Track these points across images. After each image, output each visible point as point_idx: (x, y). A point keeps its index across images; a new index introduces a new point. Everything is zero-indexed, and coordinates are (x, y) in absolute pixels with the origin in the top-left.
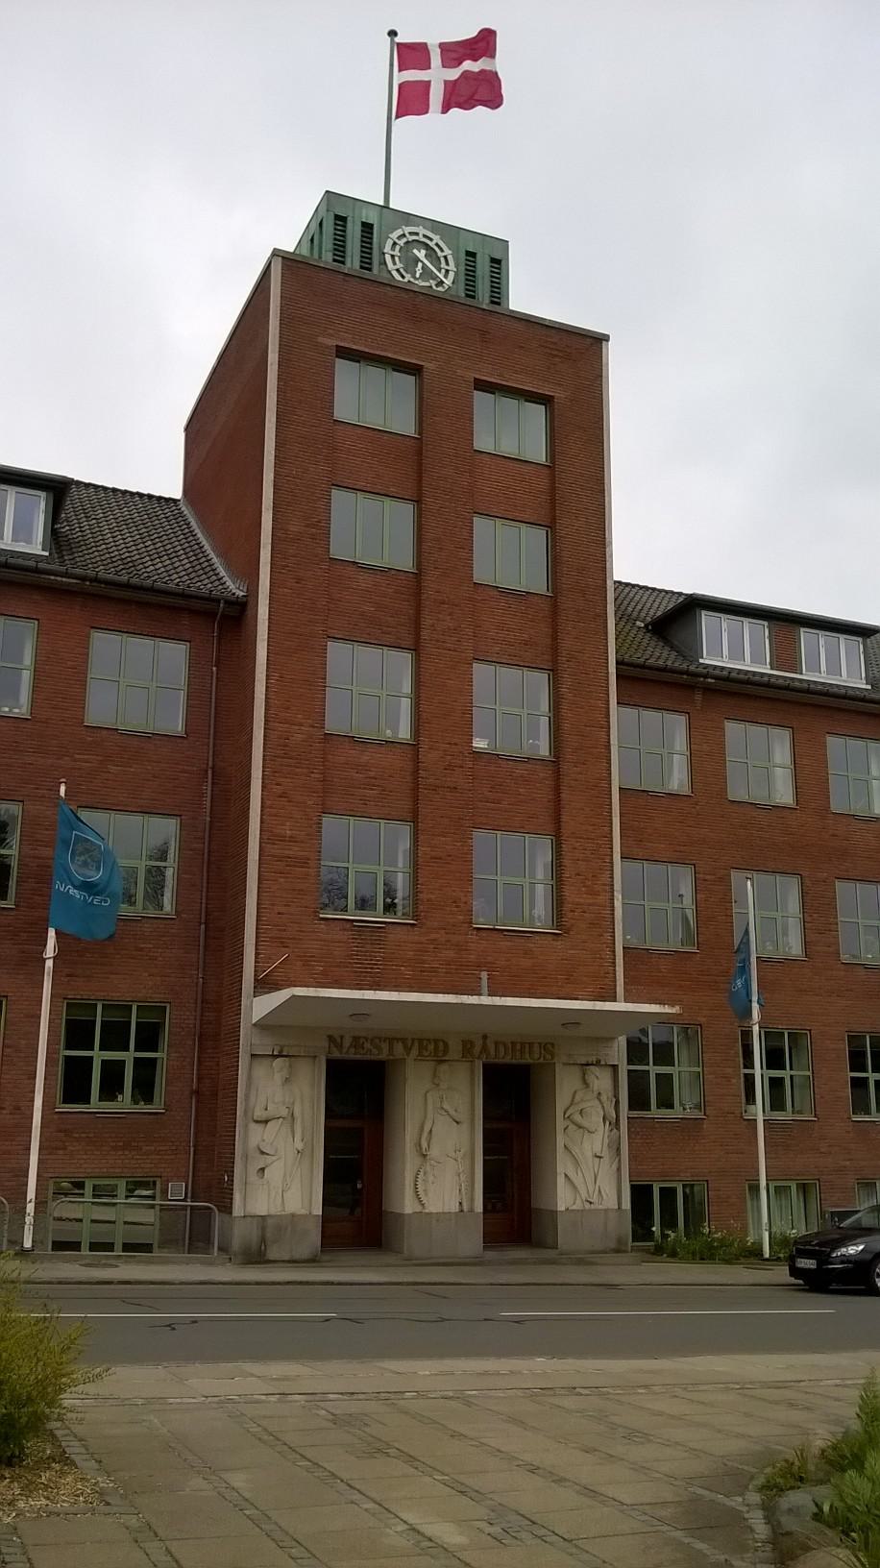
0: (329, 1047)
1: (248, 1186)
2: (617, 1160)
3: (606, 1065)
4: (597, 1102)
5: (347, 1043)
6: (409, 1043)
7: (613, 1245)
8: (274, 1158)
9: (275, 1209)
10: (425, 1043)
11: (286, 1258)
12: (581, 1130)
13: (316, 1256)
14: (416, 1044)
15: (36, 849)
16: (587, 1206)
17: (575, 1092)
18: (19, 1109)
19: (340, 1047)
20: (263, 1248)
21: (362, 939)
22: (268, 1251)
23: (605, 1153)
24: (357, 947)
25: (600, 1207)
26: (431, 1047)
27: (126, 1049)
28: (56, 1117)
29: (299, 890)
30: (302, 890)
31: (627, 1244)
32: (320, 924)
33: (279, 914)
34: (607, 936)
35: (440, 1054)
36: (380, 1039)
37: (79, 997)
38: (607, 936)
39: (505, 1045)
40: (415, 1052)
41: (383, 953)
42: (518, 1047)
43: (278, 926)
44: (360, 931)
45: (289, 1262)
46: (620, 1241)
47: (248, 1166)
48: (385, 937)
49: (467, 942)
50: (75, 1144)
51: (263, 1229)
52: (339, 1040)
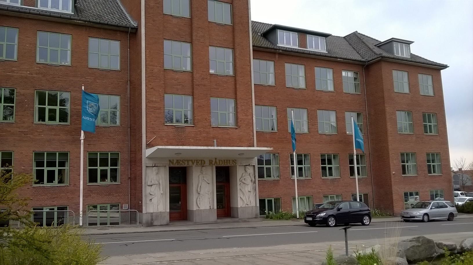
0: (170, 163)
4: (249, 176)
5: (175, 162)
6: (193, 161)
7: (254, 216)
8: (155, 196)
10: (198, 161)
12: (245, 184)
13: (168, 223)
14: (196, 161)
15: (75, 106)
16: (247, 206)
20: (152, 222)
22: (154, 223)
23: (252, 191)
26: (200, 162)
33: (153, 124)
35: (203, 164)
36: (185, 160)
40: (195, 164)
42: (226, 161)
44: (177, 129)
45: (160, 225)
46: (256, 215)
51: (152, 216)
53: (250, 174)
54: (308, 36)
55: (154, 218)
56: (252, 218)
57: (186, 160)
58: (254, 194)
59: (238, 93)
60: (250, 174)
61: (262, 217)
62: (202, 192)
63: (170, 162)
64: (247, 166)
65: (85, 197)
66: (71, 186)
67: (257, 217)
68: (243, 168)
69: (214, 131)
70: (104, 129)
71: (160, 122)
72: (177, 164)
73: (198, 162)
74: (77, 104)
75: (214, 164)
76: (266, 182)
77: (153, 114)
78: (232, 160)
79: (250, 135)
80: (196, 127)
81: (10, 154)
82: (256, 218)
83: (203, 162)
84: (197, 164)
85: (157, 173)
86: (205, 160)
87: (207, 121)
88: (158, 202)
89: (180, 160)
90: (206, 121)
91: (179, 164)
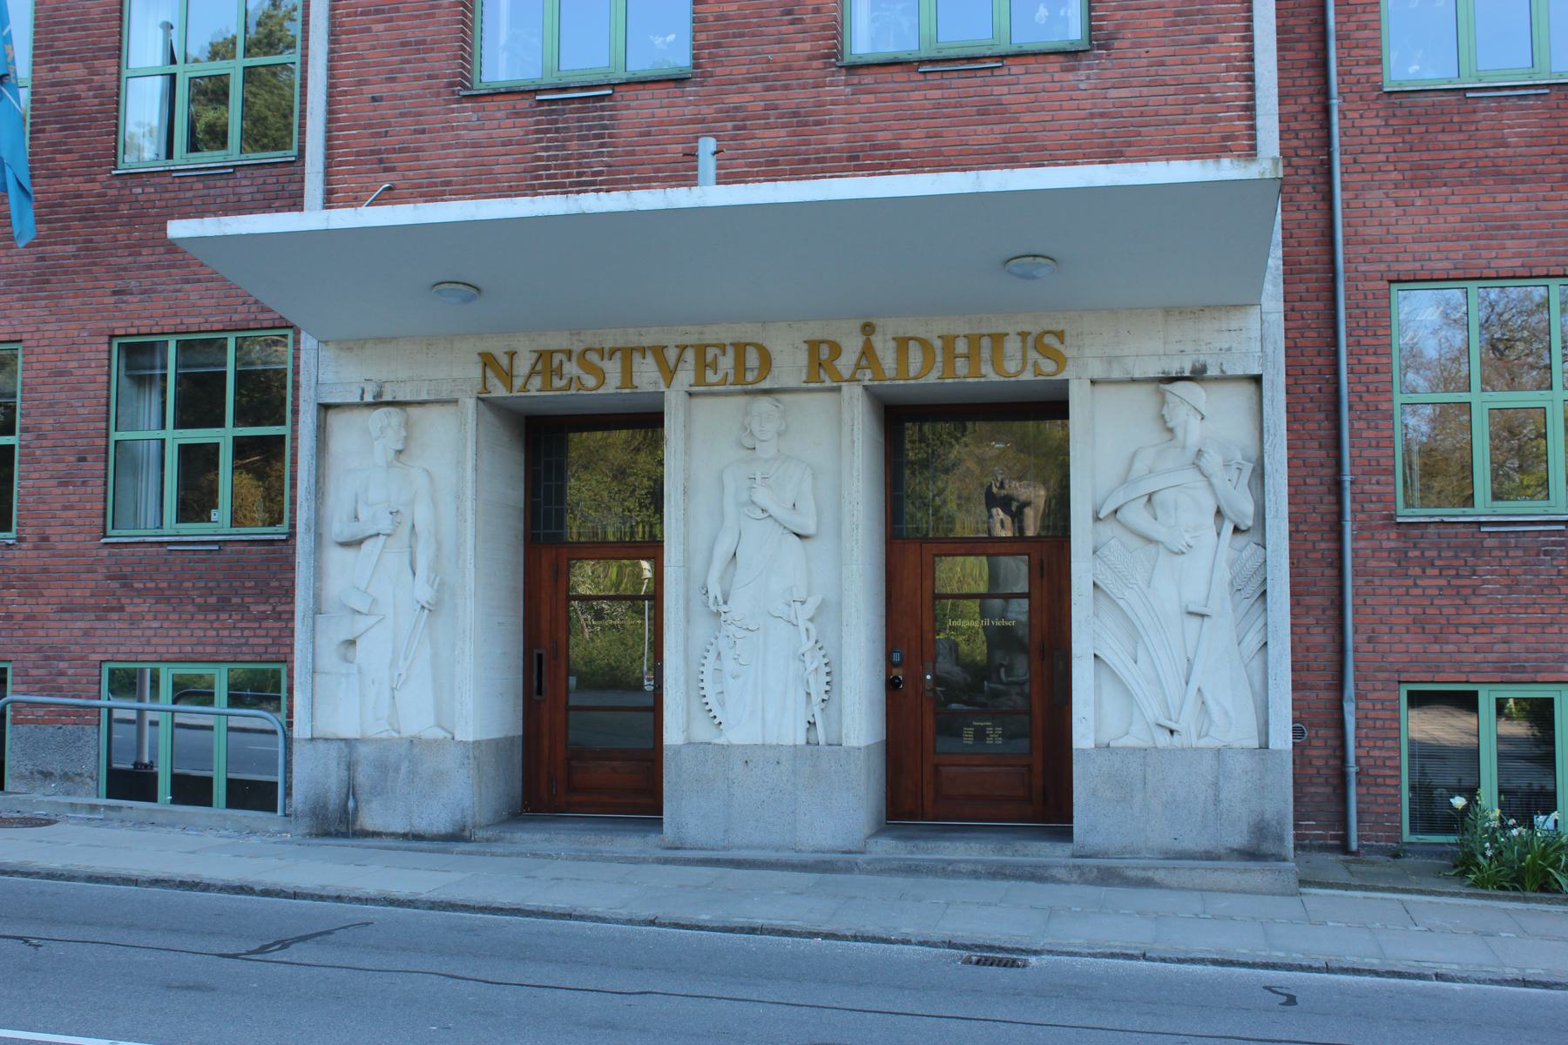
0: (485, 377)
1: (318, 678)
2: (1260, 624)
3: (1224, 378)
4: (1191, 476)
5: (523, 366)
6: (671, 355)
7: (1239, 839)
8: (372, 620)
9: (377, 729)
10: (711, 353)
11: (401, 830)
12: (1152, 548)
13: (463, 829)
14: (690, 355)
15: (57, 69)
16: (1163, 740)
17: (1134, 456)
18: (45, 539)
19: (507, 377)
20: (351, 804)
21: (557, 131)
22: (361, 814)
23: (1222, 606)
24: (546, 149)
25: (1203, 743)
26: (727, 363)
27: (220, 423)
28: (105, 552)
29: (418, 43)
30: (423, 42)
31: (1280, 839)
32: (464, 110)
33: (374, 99)
34: (1230, 42)
35: (750, 377)
36: (601, 352)
37: (134, 331)
38: (1230, 42)
39: (925, 344)
40: (685, 377)
41: (610, 154)
42: (961, 347)
43: (371, 126)
44: (552, 112)
45: (405, 836)
46: (1261, 829)
47: (318, 637)
48: (611, 118)
49: (821, 104)
50: (136, 600)
51: (350, 766)
52: (504, 361)
53: (1200, 453)
55: (363, 778)
56: (1209, 856)
57: (613, 352)
58: (1252, 641)
60: (1200, 453)
61: (1430, 854)
62: (740, 607)
63: (489, 373)
64: (1178, 387)
65: (92, 616)
66: (24, 545)
67: (1268, 847)
69: (863, 97)
70: (201, 185)
71: (430, 77)
72: (537, 382)
73: (714, 366)
74: (64, 53)
75: (846, 374)
76: (1490, 542)
77: (381, 26)
78: (1023, 335)
79: (1215, 101)
80: (701, 84)
83: (752, 359)
84: (700, 380)
85: (400, 452)
86: (767, 344)
87: (801, 21)
88: (393, 664)
89: (569, 354)
90: (793, 22)
91: (557, 383)
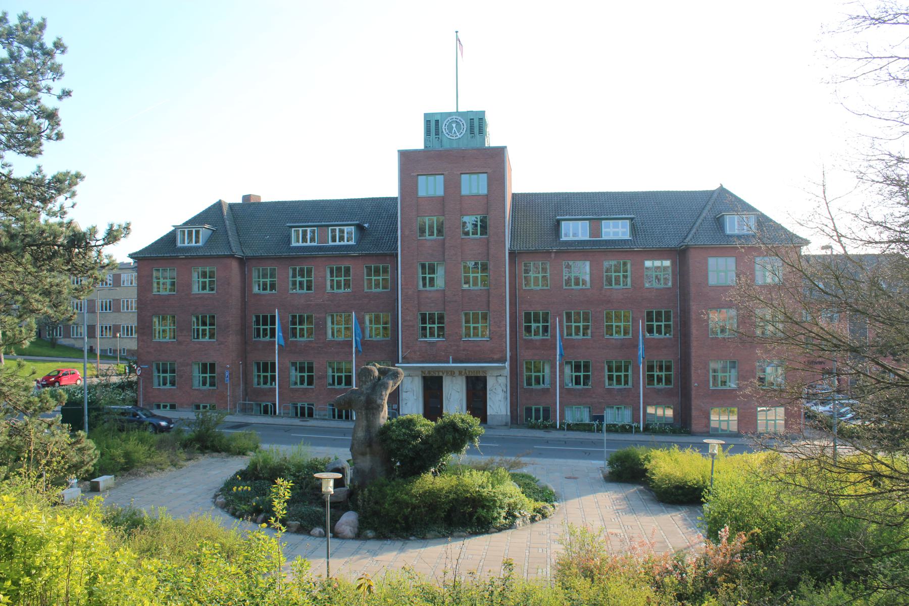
5: (426, 372)
7: (504, 424)
23: (502, 400)
40: (445, 374)
54: (111, 478)
59: (490, 305)
62: (451, 400)
68: (495, 378)
81: (312, 363)
82: (506, 425)
